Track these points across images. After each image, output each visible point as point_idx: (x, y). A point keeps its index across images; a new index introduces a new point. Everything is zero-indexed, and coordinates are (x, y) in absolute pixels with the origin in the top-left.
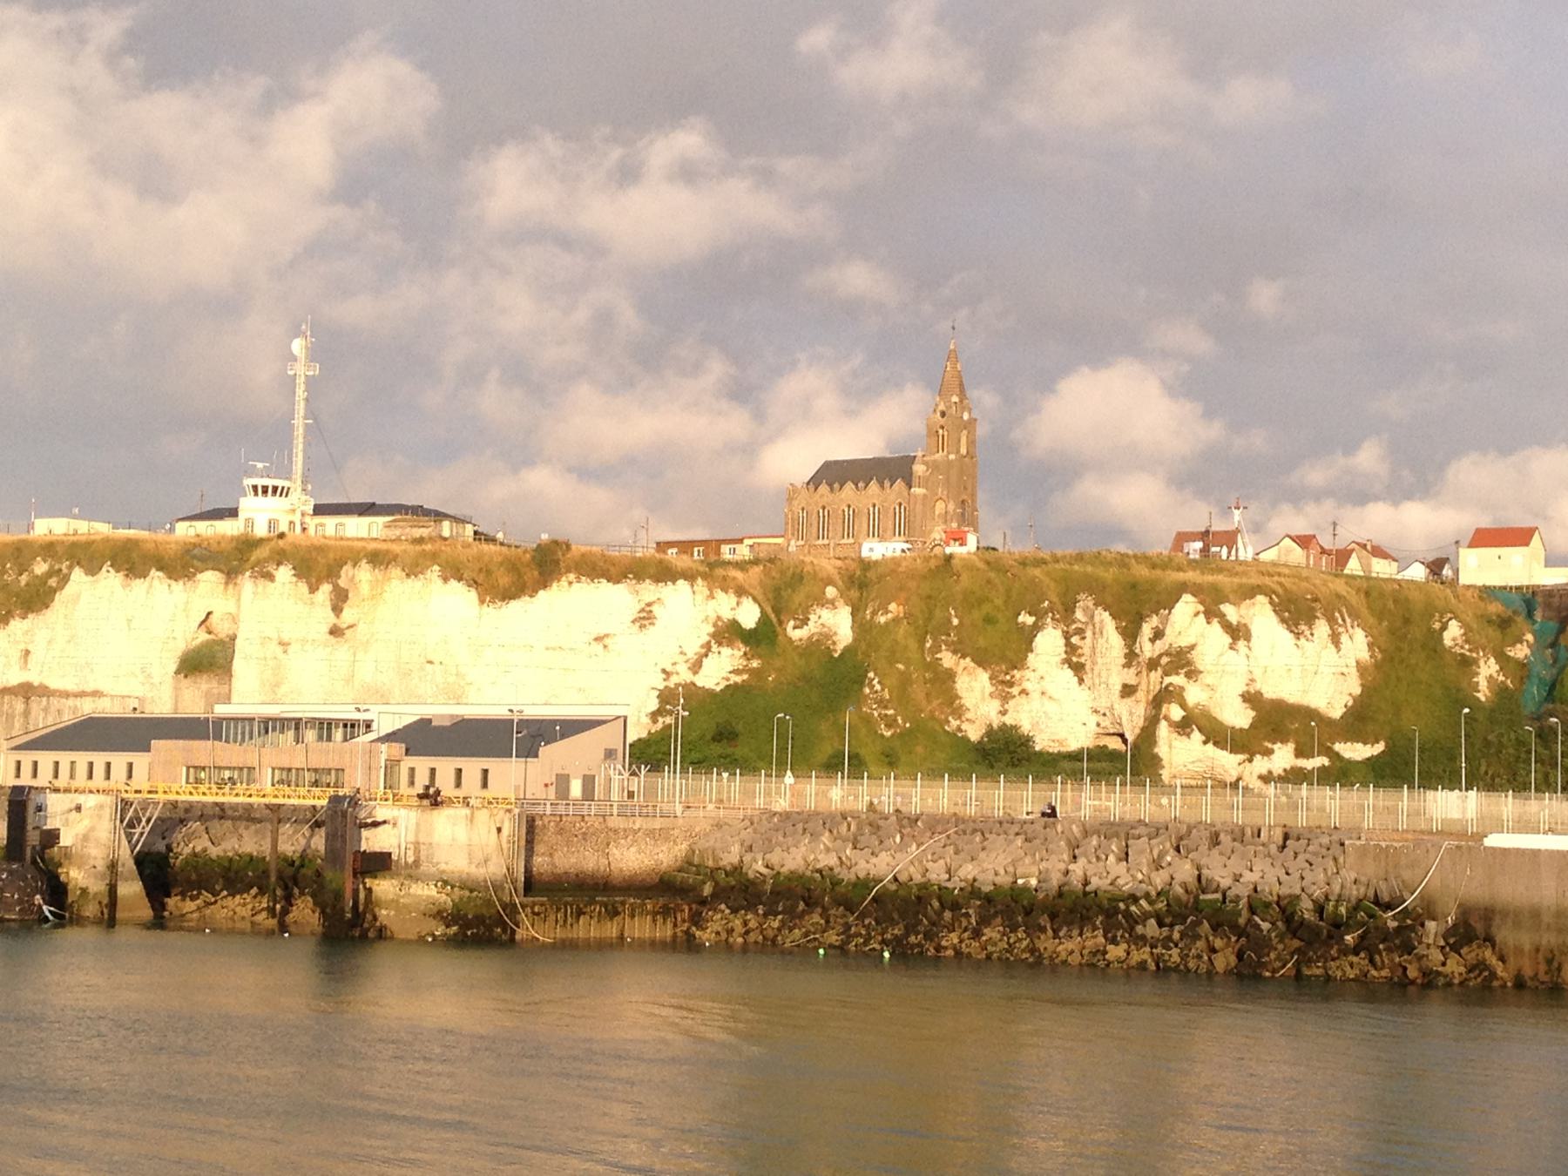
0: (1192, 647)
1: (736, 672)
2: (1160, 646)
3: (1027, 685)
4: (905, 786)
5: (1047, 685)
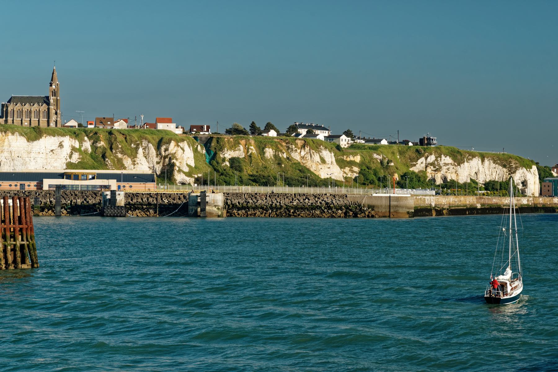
0: (175, 153)
1: (79, 159)
2: (167, 153)
3: (138, 162)
4: (321, 189)
5: (141, 162)
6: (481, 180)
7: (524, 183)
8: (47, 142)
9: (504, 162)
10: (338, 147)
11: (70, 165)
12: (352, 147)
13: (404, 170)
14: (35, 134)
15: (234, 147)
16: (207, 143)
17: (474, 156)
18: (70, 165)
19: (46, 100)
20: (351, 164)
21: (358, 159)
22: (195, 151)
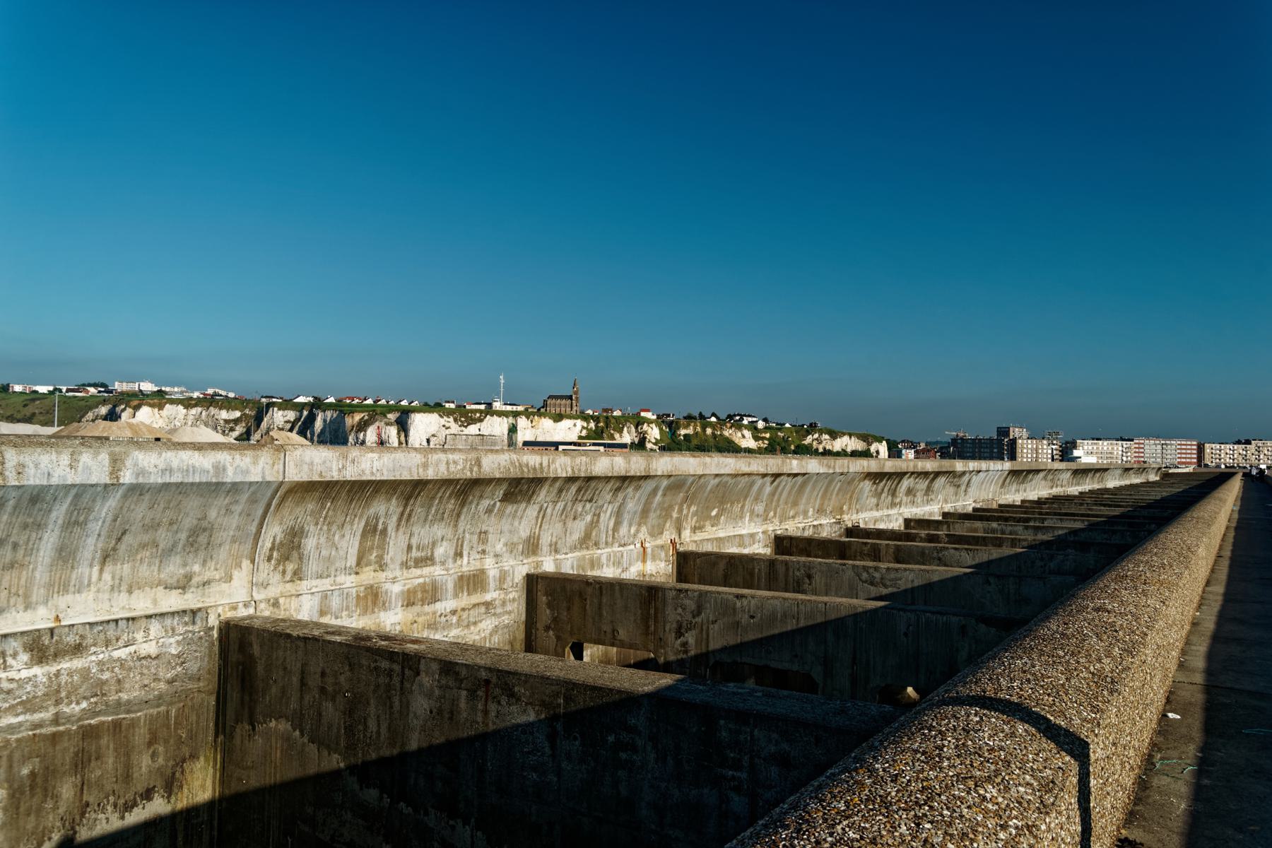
6: (849, 450)
7: (878, 452)
8: (566, 423)
9: (864, 438)
10: (756, 428)
11: (580, 437)
12: (766, 428)
13: (797, 442)
14: (558, 418)
15: (686, 427)
16: (670, 425)
17: (844, 434)
18: (580, 437)
19: (570, 397)
20: (763, 438)
21: (768, 435)
22: (661, 430)
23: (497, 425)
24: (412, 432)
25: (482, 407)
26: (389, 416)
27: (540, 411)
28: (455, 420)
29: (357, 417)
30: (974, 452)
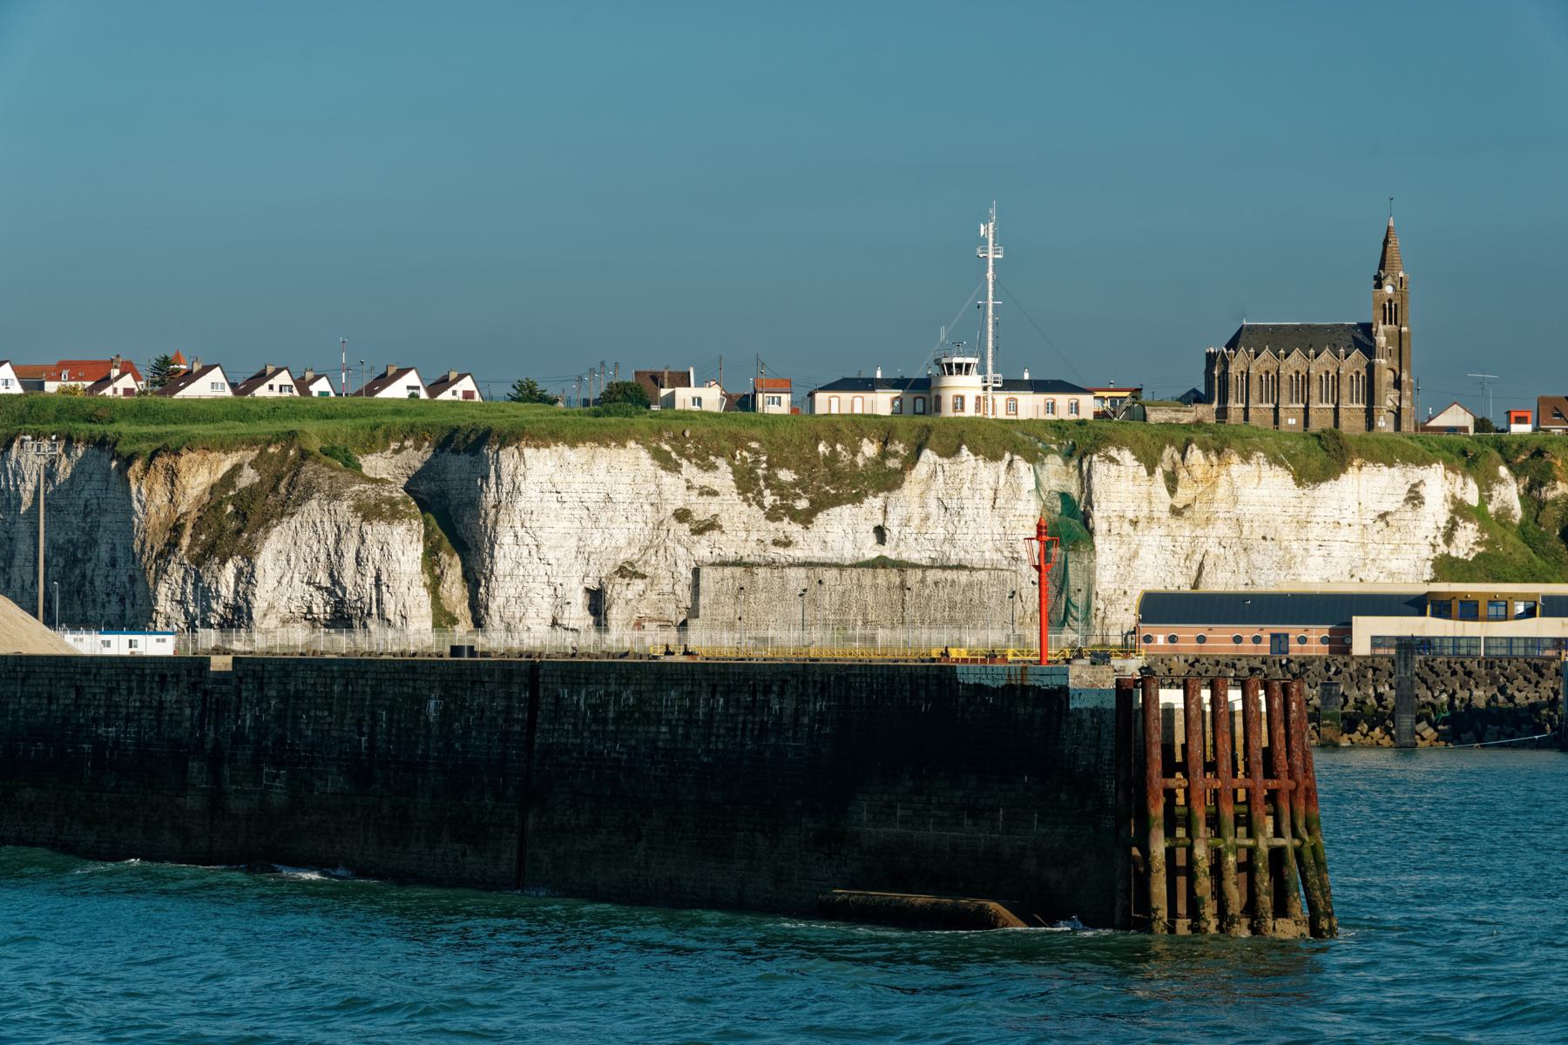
8: (1367, 487)
11: (1446, 567)
14: (1321, 457)
18: (1446, 567)
19: (1363, 338)
23: (976, 506)
24: (506, 555)
25: (881, 403)
26: (376, 464)
27: (1205, 405)
28: (746, 483)
29: (198, 476)
30: (122, 616)
